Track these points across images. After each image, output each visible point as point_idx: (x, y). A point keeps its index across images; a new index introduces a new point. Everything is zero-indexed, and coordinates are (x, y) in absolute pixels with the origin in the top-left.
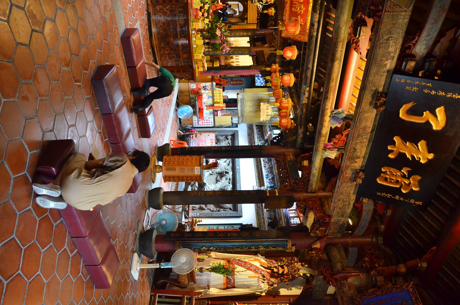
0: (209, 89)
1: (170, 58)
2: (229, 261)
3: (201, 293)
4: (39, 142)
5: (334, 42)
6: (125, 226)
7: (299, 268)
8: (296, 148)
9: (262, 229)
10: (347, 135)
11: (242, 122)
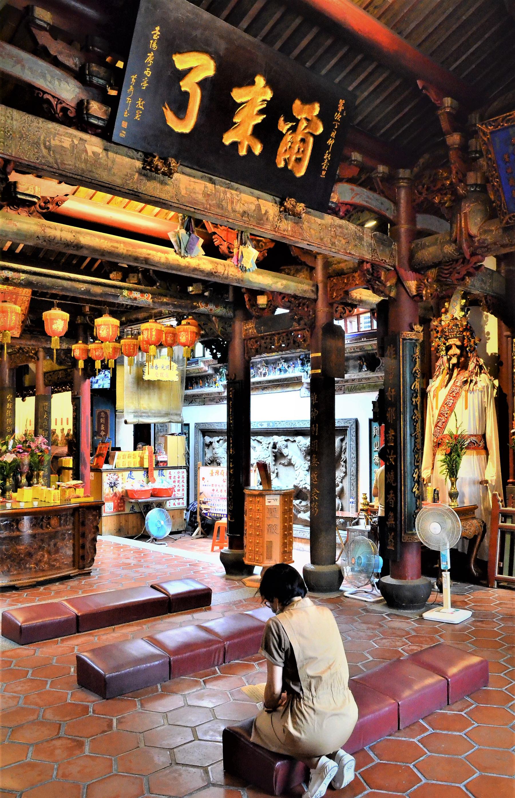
0: (115, 477)
1: (57, 551)
2: (438, 445)
3: (494, 496)
4: (228, 792)
5: (45, 244)
6: (376, 636)
7: (450, 318)
8: (235, 316)
9: (381, 381)
10: (216, 225)
11: (180, 415)
